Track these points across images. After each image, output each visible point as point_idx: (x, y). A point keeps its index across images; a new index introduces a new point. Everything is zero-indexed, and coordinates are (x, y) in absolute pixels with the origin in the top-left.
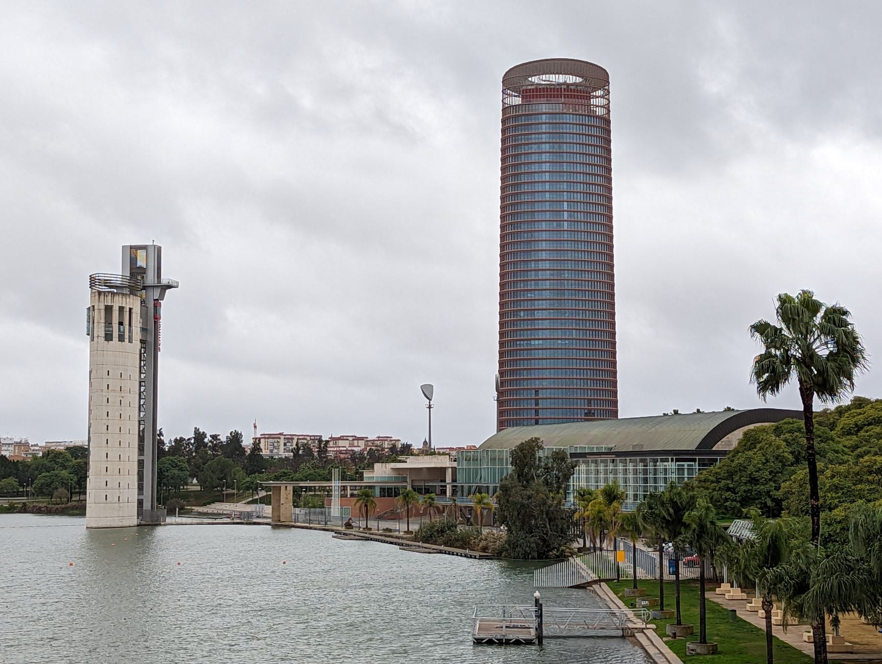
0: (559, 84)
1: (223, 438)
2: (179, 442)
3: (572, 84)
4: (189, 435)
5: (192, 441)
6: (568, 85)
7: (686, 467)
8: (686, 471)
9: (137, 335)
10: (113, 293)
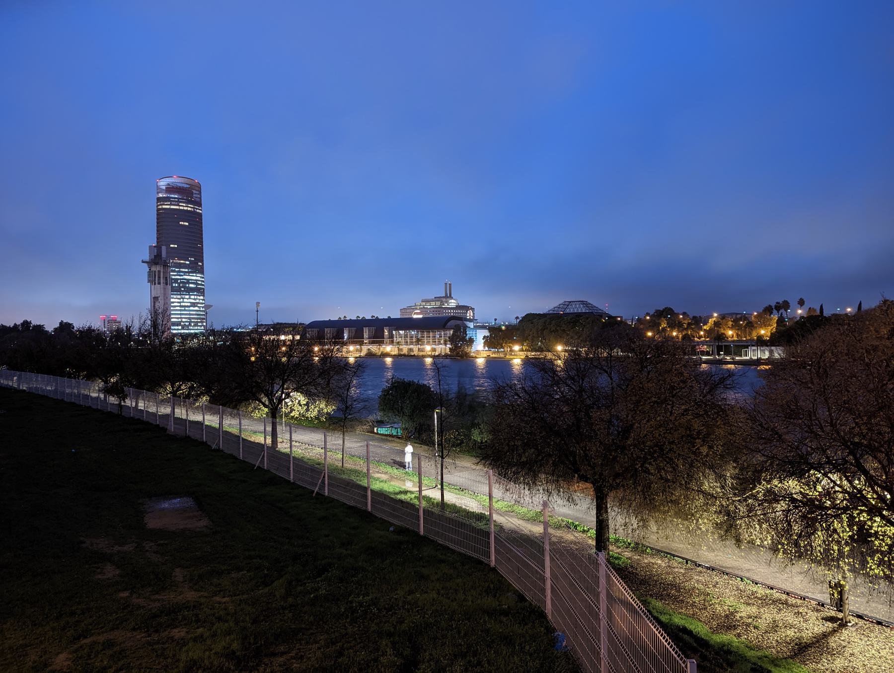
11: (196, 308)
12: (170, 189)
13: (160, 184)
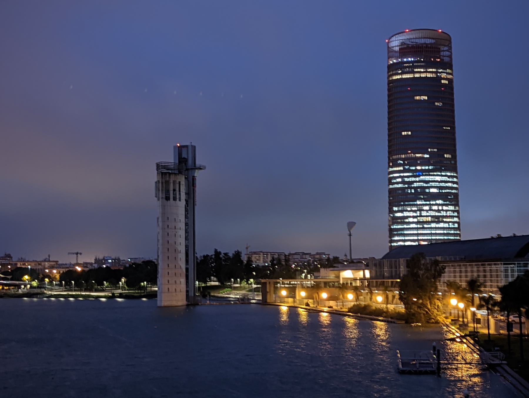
0: (422, 44)
1: (231, 255)
2: (206, 257)
3: (429, 44)
4: (211, 253)
5: (213, 257)
6: (427, 44)
7: (510, 269)
8: (510, 271)
9: (183, 196)
10: (169, 173)
11: (441, 225)
12: (406, 49)
13: (392, 44)
